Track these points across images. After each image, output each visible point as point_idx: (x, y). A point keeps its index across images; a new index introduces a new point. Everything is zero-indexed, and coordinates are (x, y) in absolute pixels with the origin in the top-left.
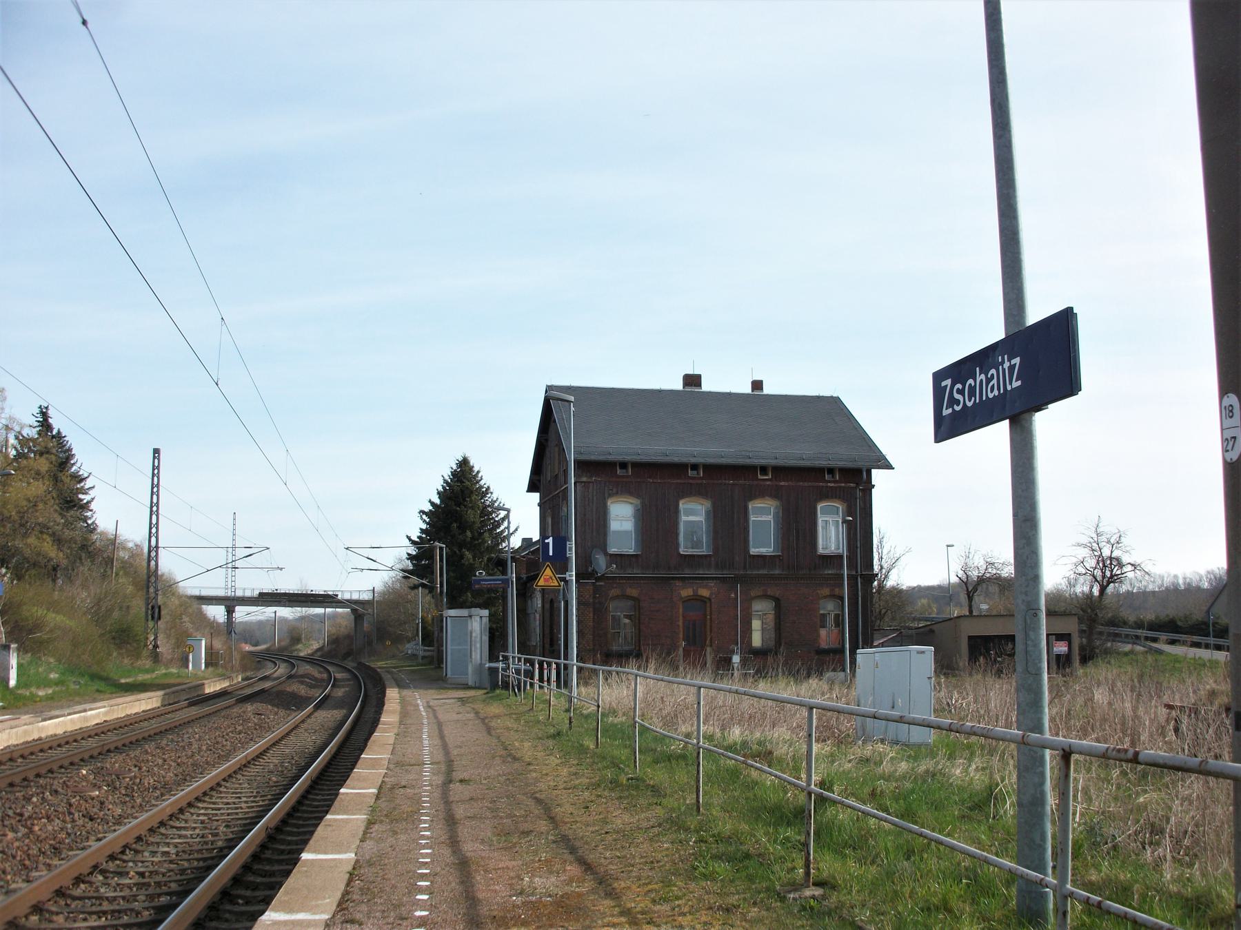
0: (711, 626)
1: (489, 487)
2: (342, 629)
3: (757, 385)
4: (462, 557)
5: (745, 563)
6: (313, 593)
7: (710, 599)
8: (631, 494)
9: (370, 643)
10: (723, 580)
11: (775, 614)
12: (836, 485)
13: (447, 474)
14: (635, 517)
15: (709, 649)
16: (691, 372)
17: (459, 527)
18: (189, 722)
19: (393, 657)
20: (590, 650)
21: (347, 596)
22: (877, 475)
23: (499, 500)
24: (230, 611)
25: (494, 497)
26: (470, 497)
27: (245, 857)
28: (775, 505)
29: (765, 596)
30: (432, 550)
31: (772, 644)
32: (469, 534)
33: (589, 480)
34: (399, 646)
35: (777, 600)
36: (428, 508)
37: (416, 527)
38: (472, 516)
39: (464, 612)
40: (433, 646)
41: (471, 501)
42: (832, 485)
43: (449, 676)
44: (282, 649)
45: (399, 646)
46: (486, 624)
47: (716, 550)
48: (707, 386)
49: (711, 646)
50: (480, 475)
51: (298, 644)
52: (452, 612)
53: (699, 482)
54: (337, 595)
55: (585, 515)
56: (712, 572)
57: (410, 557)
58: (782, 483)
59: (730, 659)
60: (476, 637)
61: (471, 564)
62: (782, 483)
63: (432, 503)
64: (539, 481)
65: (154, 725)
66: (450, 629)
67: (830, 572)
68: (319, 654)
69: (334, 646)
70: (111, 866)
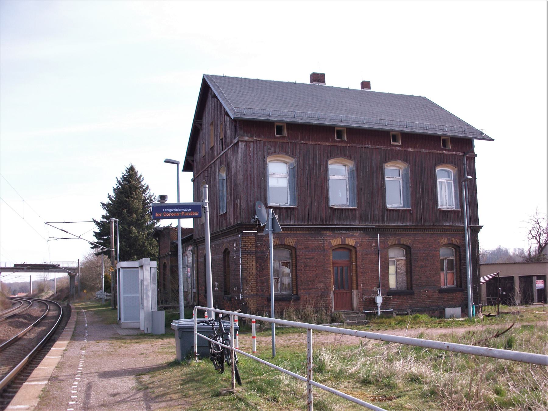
0: (356, 271)
1: (148, 185)
2: (65, 284)
4: (130, 232)
5: (383, 216)
6: (46, 264)
7: (355, 247)
8: (287, 153)
9: (77, 292)
10: (365, 230)
11: (406, 260)
12: (449, 153)
14: (289, 175)
15: (355, 292)
16: (317, 71)
17: (128, 212)
19: (89, 300)
20: (253, 296)
21: (65, 266)
22: (478, 144)
23: (154, 195)
26: (135, 191)
28: (403, 167)
29: (399, 245)
31: (404, 286)
32: (135, 216)
33: (251, 140)
34: (93, 293)
36: (106, 201)
37: (100, 214)
40: (110, 293)
41: (136, 194)
42: (446, 153)
43: (122, 321)
44: (34, 296)
45: (93, 293)
46: (154, 274)
47: (359, 203)
49: (357, 289)
50: (142, 178)
51: (42, 292)
52: (124, 264)
53: (344, 145)
54: (59, 265)
55: (247, 171)
56: (357, 224)
57: (96, 234)
58: (410, 149)
59: (374, 299)
60: (147, 286)
61: (136, 236)
62: (410, 149)
64: (193, 161)
67: (448, 224)
68: (52, 298)
69: (60, 294)
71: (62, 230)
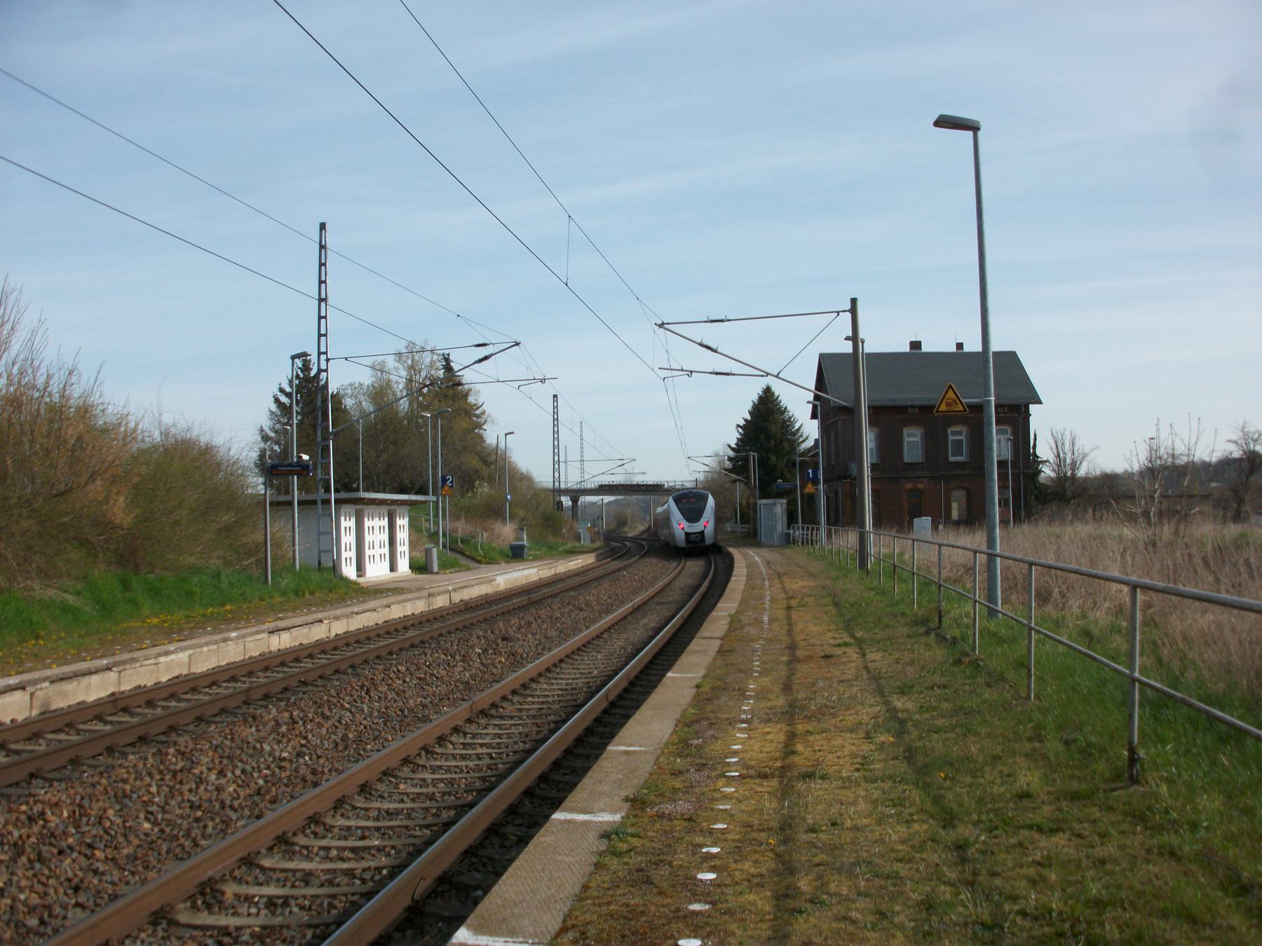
3: (960, 346)
4: (768, 459)
13: (755, 398)
18: (619, 570)
22: (1033, 408)
24: (575, 501)
25: (791, 414)
27: (579, 730)
30: (746, 459)
32: (773, 442)
35: (968, 490)
38: (774, 429)
39: (771, 501)
48: (925, 349)
52: (764, 501)
63: (746, 420)
65: (592, 575)
66: (763, 513)
70: (493, 712)
71: (701, 345)
